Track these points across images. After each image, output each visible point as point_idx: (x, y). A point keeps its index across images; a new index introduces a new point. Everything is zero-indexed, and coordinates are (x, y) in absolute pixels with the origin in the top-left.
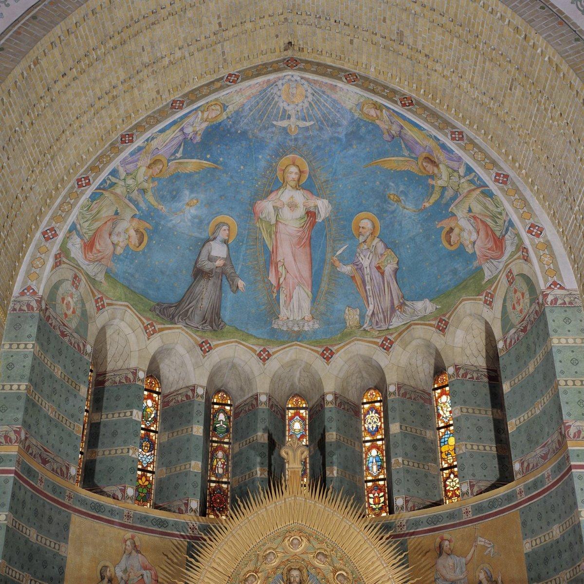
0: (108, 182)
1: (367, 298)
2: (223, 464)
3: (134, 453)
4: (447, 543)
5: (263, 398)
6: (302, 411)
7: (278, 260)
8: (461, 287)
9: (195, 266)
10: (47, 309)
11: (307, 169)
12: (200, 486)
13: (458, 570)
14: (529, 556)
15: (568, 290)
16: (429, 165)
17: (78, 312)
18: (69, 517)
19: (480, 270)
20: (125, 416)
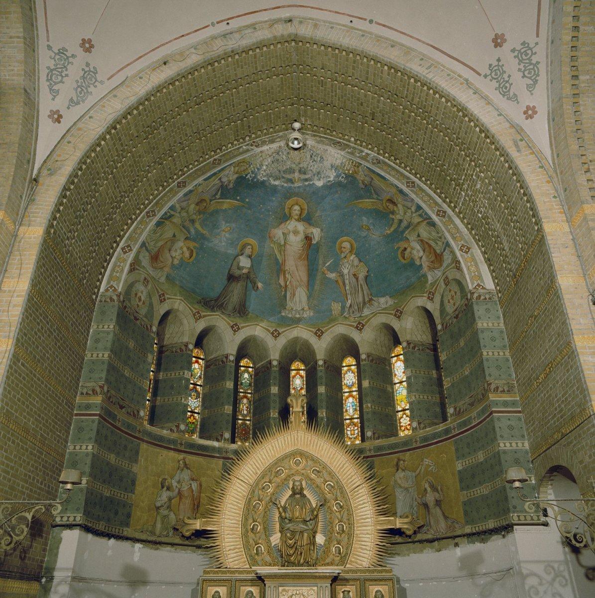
5: (275, 363)
9: (229, 273)
11: (306, 207)
17: (147, 303)
18: (139, 445)
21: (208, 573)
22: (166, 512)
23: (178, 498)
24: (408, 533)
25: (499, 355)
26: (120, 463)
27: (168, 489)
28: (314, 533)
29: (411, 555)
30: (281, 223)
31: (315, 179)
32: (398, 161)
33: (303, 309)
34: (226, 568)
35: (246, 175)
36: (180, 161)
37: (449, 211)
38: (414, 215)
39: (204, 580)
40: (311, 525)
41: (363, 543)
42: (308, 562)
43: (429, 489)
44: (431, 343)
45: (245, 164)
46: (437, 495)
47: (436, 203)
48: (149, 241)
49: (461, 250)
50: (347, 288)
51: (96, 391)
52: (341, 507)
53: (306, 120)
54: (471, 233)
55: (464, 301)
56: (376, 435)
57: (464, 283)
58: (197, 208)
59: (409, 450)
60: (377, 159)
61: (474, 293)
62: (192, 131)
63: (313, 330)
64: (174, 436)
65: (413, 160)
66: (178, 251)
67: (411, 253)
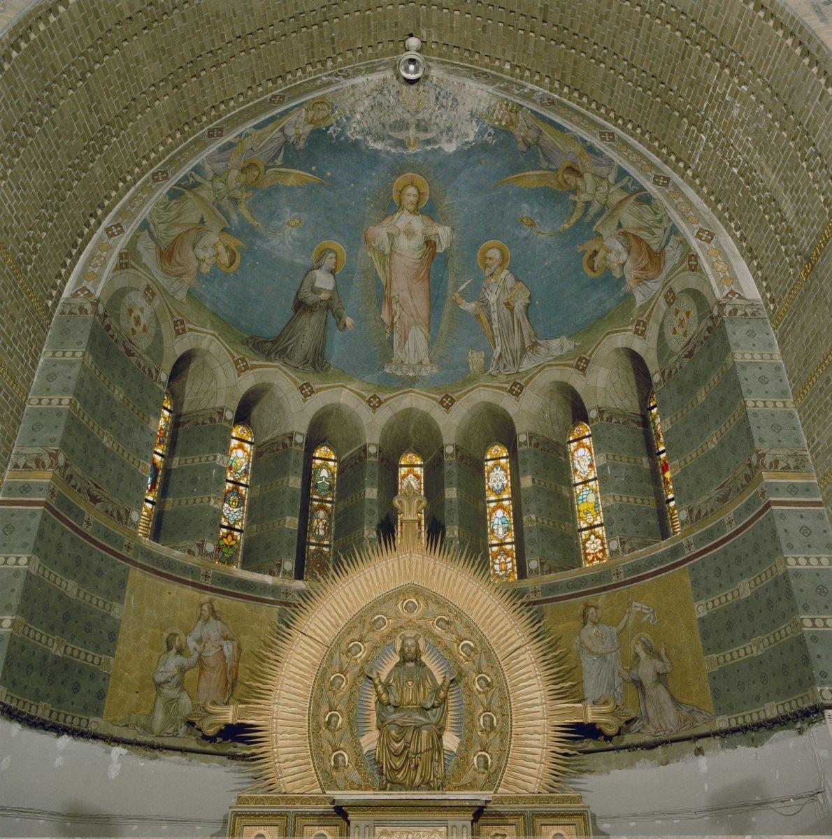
0: (191, 179)
1: (494, 339)
2: (325, 525)
5: (373, 450)
6: (416, 469)
7: (392, 295)
8: (606, 318)
9: (296, 298)
10: (106, 316)
11: (428, 191)
14: (703, 621)
15: (749, 300)
16: (571, 177)
17: (152, 331)
18: (126, 571)
19: (629, 296)
21: (246, 801)
22: (174, 693)
23: (197, 669)
24: (609, 731)
25: (775, 406)
26: (88, 598)
27: (180, 652)
28: (439, 730)
29: (612, 772)
30: (386, 216)
31: (443, 140)
32: (585, 99)
33: (421, 363)
35: (328, 128)
36: (213, 87)
37: (675, 177)
38: (612, 189)
39: (237, 815)
40: (435, 716)
41: (529, 749)
42: (428, 783)
43: (643, 655)
44: (639, 412)
45: (326, 107)
46: (659, 664)
47: (652, 165)
48: (156, 222)
49: (698, 236)
50: (495, 326)
51: (43, 463)
52: (488, 685)
53: (429, 34)
54: (714, 210)
55: (707, 323)
57: (704, 291)
58: (243, 178)
59: (605, 589)
60: (549, 99)
61: (724, 305)
62: (233, 31)
63: (437, 397)
64: (194, 561)
65: (613, 92)
66: (210, 250)
67: (605, 258)
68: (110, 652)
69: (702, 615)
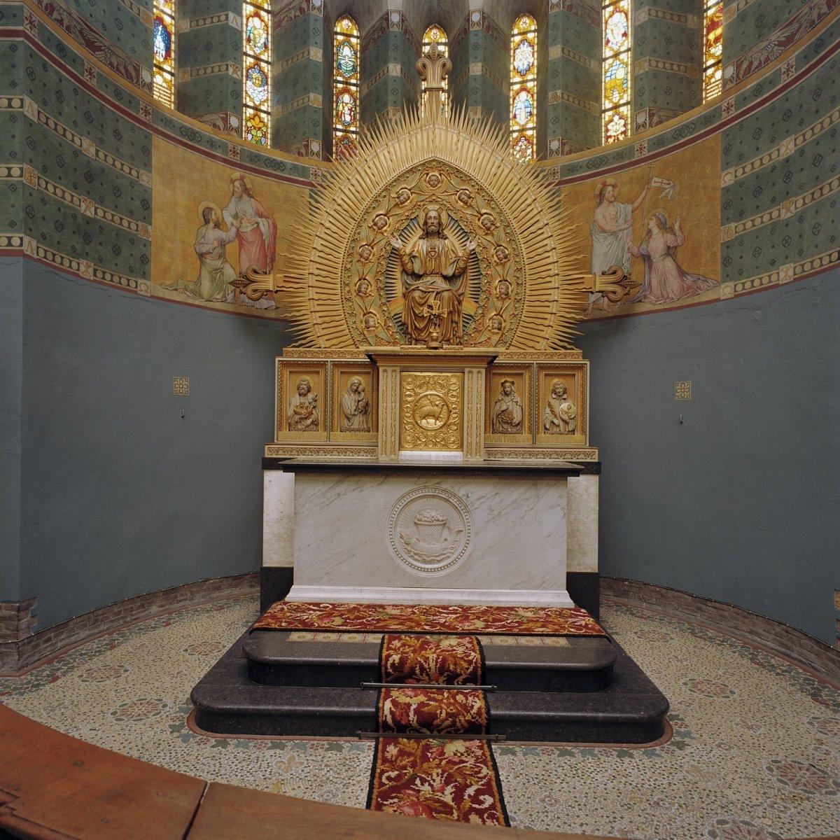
3: (234, 72)
4: (610, 189)
5: (395, 18)
12: (321, 125)
13: (621, 220)
18: (147, 136)
20: (219, 21)
22: (218, 264)
27: (217, 226)
34: (320, 347)
43: (655, 231)
46: (669, 236)
56: (567, 148)
68: (147, 219)
69: (728, 183)
